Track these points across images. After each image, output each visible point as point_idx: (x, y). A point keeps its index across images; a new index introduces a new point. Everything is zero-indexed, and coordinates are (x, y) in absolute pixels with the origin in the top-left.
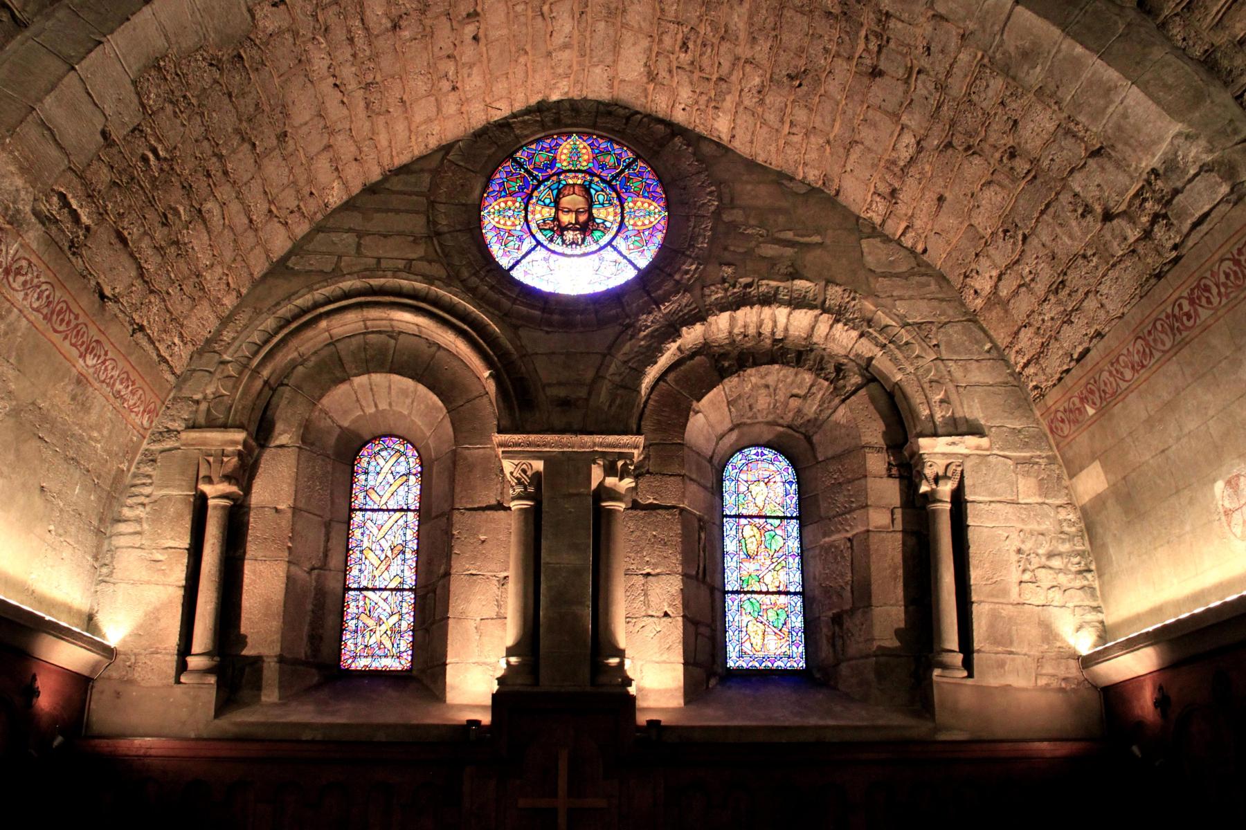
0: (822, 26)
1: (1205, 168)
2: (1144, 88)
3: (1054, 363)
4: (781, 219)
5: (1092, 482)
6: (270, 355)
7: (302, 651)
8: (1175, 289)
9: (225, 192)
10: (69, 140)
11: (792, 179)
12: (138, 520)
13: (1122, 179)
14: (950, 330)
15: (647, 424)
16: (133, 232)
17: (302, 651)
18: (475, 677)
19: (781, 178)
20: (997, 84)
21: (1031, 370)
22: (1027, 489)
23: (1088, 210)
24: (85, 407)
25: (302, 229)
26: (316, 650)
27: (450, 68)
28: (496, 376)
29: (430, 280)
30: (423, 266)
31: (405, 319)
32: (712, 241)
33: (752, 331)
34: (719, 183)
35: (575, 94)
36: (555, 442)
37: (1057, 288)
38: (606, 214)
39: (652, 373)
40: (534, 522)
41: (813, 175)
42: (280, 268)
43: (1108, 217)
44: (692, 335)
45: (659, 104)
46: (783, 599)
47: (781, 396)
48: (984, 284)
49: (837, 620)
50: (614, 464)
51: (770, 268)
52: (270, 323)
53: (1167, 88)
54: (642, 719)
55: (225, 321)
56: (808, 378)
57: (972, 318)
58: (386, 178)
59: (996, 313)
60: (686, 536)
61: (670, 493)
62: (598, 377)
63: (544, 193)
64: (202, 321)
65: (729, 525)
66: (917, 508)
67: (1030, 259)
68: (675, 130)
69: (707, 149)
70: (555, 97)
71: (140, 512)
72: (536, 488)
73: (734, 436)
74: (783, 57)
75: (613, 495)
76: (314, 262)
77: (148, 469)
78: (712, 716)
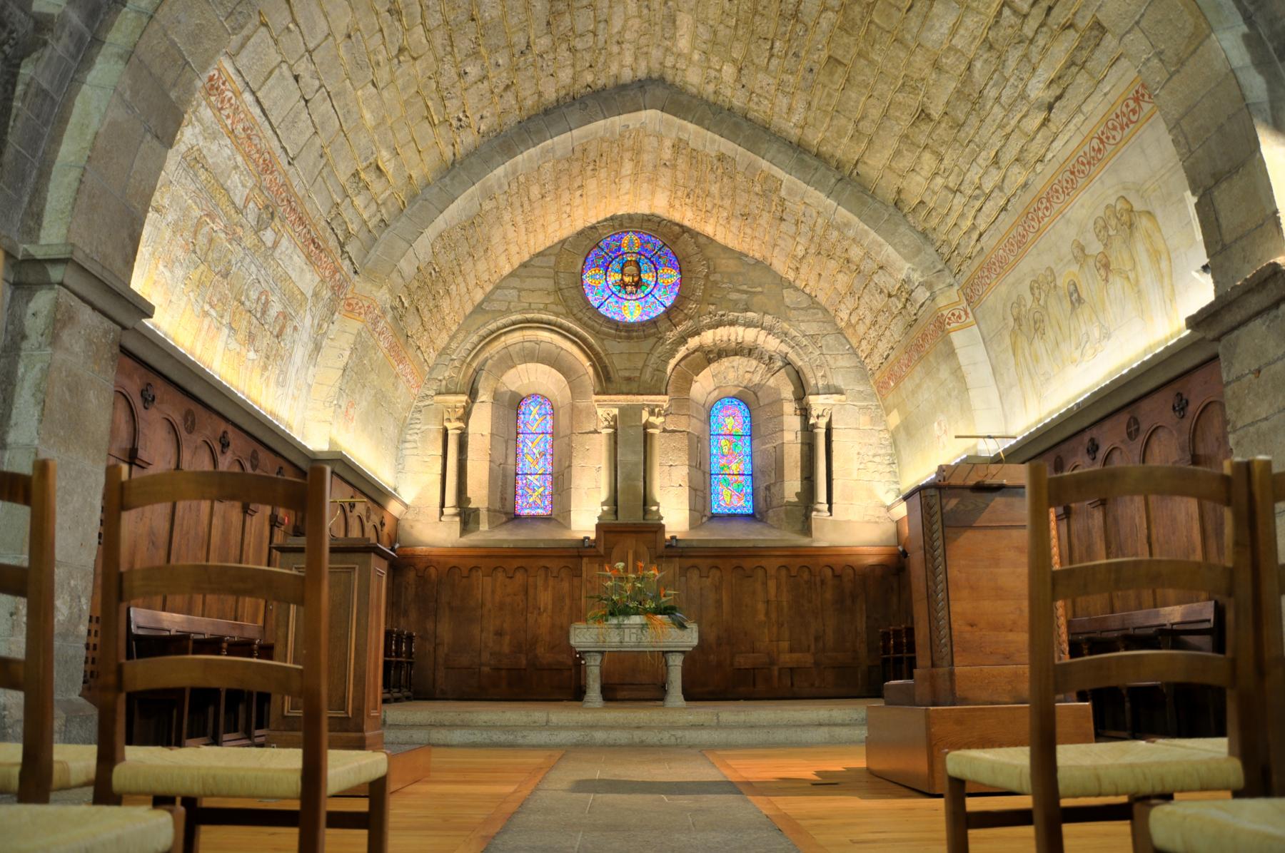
0: (754, 198)
1: (920, 284)
2: (894, 246)
3: (877, 359)
4: (741, 278)
5: (894, 419)
6: (476, 355)
7: (498, 505)
8: (916, 332)
9: (460, 279)
10: (406, 275)
11: (747, 256)
12: (415, 441)
13: (892, 281)
14: (828, 338)
15: (670, 389)
16: (422, 305)
17: (498, 505)
18: (585, 519)
19: (741, 256)
20: (836, 233)
21: (868, 361)
22: (864, 421)
23: (881, 292)
24: (397, 389)
25: (489, 288)
26: (503, 506)
27: (568, 209)
28: (594, 366)
29: (557, 314)
30: (553, 307)
31: (545, 335)
32: (704, 291)
33: (725, 338)
34: (708, 259)
35: (631, 212)
36: (623, 400)
37: (874, 323)
38: (648, 277)
39: (673, 362)
40: (614, 439)
41: (757, 255)
42: (479, 309)
43: (890, 296)
44: (693, 342)
45: (677, 217)
46: (741, 478)
47: (741, 372)
48: (844, 314)
49: (768, 488)
50: (654, 408)
51: (734, 306)
52: (475, 338)
53: (905, 246)
54: (668, 536)
55: (452, 338)
56: (754, 363)
57: (840, 332)
58: (531, 259)
59: (851, 330)
60: (690, 446)
61: (681, 424)
62: (645, 365)
63: (615, 265)
64: (442, 340)
65: (714, 439)
66: (808, 431)
67: (862, 308)
68: (684, 229)
69: (702, 240)
70: (620, 213)
71: (415, 437)
72: (615, 424)
73: (716, 393)
74: (737, 207)
75: (654, 426)
76: (496, 306)
77: (417, 415)
78: (703, 535)
